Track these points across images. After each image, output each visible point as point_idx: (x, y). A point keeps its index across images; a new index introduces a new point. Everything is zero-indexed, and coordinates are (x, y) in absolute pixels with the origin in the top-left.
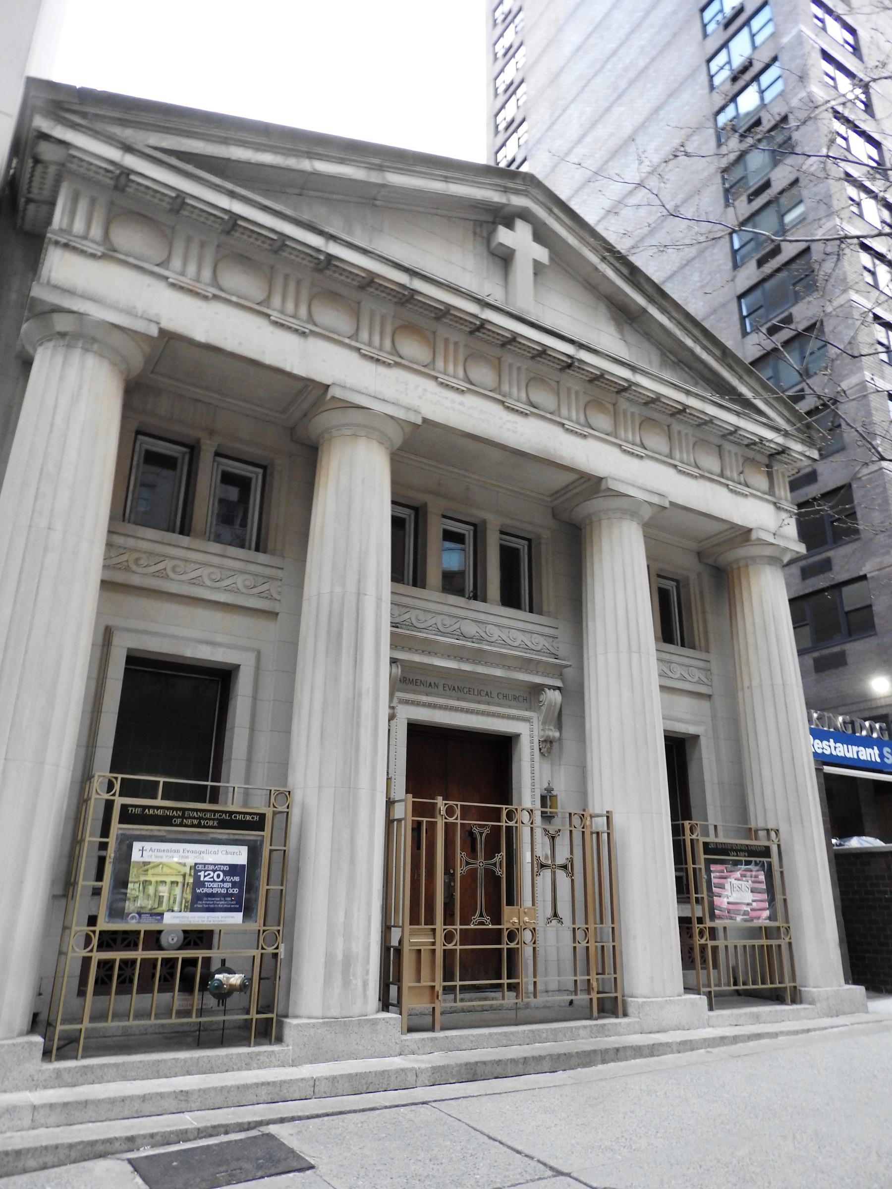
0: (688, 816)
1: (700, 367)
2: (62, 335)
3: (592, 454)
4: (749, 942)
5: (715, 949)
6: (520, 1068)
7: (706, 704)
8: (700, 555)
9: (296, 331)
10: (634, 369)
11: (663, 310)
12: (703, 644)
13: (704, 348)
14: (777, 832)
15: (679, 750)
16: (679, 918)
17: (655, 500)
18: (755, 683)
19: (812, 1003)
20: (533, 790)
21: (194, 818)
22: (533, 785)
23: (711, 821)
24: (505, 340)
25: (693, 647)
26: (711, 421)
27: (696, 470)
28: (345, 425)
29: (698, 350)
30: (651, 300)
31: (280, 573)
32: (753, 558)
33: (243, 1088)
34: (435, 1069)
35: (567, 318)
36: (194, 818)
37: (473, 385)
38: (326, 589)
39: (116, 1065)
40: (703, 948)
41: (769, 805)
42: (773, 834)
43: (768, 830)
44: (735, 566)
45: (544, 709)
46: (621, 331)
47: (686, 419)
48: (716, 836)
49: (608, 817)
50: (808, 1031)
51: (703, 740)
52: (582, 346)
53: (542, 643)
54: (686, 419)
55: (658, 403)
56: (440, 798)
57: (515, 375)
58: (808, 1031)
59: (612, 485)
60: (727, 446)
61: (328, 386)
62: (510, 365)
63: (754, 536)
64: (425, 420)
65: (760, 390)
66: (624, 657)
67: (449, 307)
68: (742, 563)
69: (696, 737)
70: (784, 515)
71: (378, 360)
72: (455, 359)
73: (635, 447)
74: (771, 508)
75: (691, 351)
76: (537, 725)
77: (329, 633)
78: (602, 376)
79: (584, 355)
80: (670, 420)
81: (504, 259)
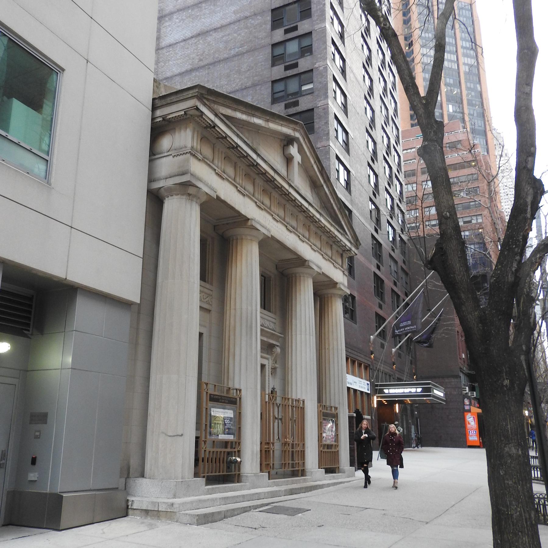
1: (332, 211)
2: (189, 195)
3: (305, 251)
6: (304, 490)
8: (215, 227)
10: (310, 204)
11: (328, 187)
13: (336, 204)
18: (331, 347)
19: (344, 472)
20: (269, 388)
22: (269, 386)
24: (220, 136)
25: (270, 311)
26: (226, 138)
29: (334, 205)
30: (325, 182)
31: (211, 293)
32: (334, 294)
33: (243, 496)
34: (285, 490)
35: (299, 185)
38: (244, 307)
39: (218, 488)
41: (332, 397)
43: (331, 407)
44: (234, 238)
45: (274, 355)
46: (311, 189)
47: (223, 142)
50: (350, 481)
53: (272, 326)
54: (223, 142)
55: (225, 140)
57: (220, 155)
58: (350, 481)
59: (254, 224)
60: (334, 246)
61: (249, 219)
62: (240, 167)
63: (249, 223)
64: (218, 198)
65: (235, 106)
66: (308, 336)
67: (238, 146)
68: (329, 295)
70: (345, 276)
72: (218, 159)
74: (342, 273)
75: (332, 205)
76: (271, 361)
77: (247, 326)
78: (226, 138)
79: (310, 209)
80: (322, 234)
81: (289, 160)
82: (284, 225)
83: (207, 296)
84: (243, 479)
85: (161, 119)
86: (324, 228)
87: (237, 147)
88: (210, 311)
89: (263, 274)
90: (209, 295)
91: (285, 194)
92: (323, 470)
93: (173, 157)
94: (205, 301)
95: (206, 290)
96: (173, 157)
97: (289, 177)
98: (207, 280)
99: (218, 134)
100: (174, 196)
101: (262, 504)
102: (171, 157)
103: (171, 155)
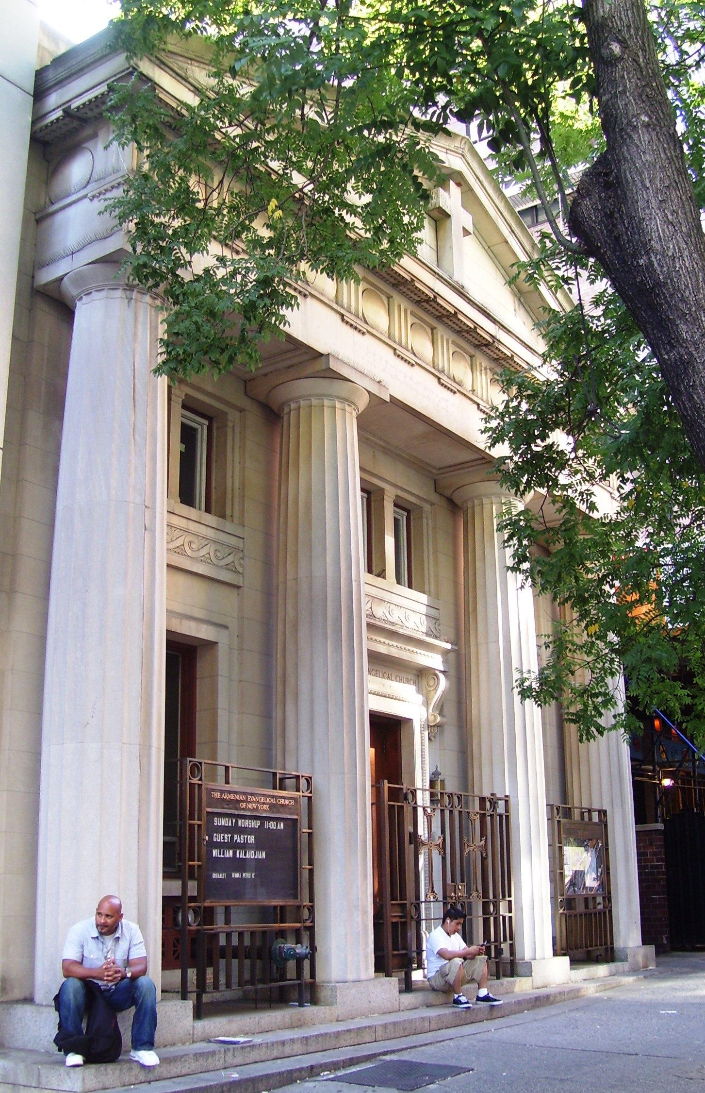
0: (189, 751)
4: (258, 926)
5: (510, 918)
7: (233, 594)
9: (351, 325)
12: (236, 514)
14: (309, 780)
15: (184, 659)
16: (163, 897)
17: (375, 390)
19: (625, 960)
21: (254, 802)
23: (222, 759)
27: (412, 356)
28: (325, 395)
36: (254, 802)
37: (367, 323)
40: (504, 918)
42: (303, 783)
48: (227, 782)
49: (506, 801)
51: (222, 652)
52: (502, 327)
56: (386, 781)
59: (333, 365)
61: (322, 355)
69: (211, 645)
71: (356, 328)
73: (358, 321)
79: (502, 336)
82: (475, 402)
83: (228, 551)
84: (323, 994)
85: (59, 113)
86: (434, 300)
87: (475, 328)
88: (239, 587)
89: (367, 487)
90: (234, 550)
91: (428, 300)
92: (567, 959)
93: (91, 200)
94: (223, 563)
95: (182, 523)
96: (91, 200)
97: (445, 263)
98: (228, 512)
99: (441, 310)
100: (95, 295)
101: (351, 1059)
102: (87, 200)
103: (85, 196)
